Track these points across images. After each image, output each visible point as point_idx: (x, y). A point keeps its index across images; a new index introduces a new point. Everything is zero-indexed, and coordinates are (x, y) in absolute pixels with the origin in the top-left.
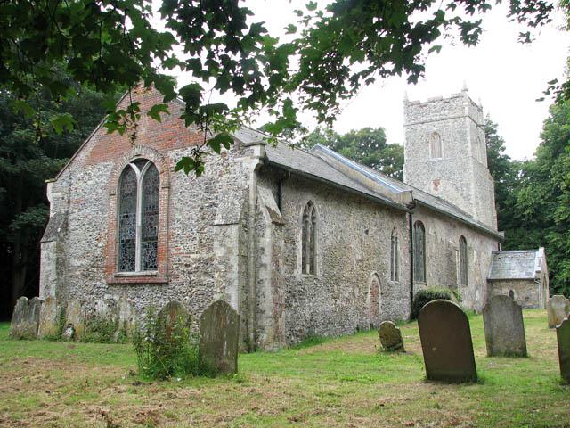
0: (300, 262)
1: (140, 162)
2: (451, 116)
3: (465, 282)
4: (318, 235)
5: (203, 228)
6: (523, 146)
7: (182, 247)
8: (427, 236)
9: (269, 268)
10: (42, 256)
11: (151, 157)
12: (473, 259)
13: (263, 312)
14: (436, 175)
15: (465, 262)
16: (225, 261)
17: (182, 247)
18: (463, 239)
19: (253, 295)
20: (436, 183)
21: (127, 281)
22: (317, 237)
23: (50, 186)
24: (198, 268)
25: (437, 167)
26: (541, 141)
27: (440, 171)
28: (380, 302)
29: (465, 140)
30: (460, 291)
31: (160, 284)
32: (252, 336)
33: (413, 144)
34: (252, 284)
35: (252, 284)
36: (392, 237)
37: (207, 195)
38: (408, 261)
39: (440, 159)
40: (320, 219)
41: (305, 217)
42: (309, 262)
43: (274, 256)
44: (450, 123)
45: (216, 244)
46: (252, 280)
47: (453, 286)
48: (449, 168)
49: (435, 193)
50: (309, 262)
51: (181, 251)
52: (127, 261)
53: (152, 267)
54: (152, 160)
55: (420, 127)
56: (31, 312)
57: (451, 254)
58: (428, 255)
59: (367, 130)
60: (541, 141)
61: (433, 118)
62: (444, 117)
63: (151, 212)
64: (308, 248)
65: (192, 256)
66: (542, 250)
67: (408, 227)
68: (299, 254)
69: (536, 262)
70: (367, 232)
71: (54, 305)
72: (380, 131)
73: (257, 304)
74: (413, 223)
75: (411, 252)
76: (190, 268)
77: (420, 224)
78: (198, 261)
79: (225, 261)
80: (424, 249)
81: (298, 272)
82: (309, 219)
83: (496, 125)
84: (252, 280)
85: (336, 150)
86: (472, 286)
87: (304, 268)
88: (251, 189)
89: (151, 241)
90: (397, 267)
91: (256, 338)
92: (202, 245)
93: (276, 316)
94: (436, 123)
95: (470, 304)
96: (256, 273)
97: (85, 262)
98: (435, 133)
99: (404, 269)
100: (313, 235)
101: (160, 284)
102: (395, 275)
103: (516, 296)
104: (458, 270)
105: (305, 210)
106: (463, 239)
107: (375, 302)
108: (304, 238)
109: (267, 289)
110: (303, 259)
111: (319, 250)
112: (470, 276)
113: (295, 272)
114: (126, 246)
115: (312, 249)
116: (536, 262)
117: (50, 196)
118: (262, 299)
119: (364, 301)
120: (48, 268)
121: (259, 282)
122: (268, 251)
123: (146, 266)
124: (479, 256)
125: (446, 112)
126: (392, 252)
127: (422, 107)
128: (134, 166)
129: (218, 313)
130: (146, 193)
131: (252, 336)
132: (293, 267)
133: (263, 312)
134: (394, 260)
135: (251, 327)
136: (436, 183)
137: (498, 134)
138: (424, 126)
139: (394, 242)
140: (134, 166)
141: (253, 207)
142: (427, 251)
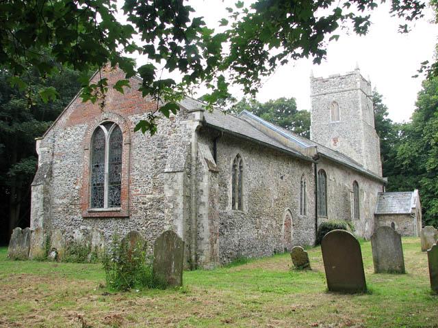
0: (230, 201)
1: (108, 124)
2: (346, 89)
3: (358, 216)
4: (245, 180)
5: (156, 175)
6: (402, 112)
7: (140, 189)
8: (328, 180)
9: (207, 206)
10: (32, 196)
11: (116, 120)
12: (363, 199)
13: (202, 239)
14: (335, 134)
15: (357, 201)
16: (173, 200)
17: (140, 189)
18: (356, 183)
19: (194, 226)
20: (335, 140)
21: (98, 216)
22: (244, 182)
23: (38, 143)
24: (152, 205)
25: (336, 128)
26: (416, 108)
27: (338, 131)
28: (292, 232)
29: (357, 107)
30: (353, 223)
31: (123, 218)
32: (193, 257)
33: (317, 110)
34: (193, 217)
35: (193, 217)
36: (302, 182)
37: (159, 150)
38: (313, 200)
39: (338, 122)
40: (246, 168)
41: (234, 166)
42: (237, 201)
43: (211, 196)
44: (346, 94)
45: (166, 187)
46: (194, 214)
47: (348, 219)
48: (345, 129)
49: (335, 148)
50: (237, 201)
51: (139, 192)
52: (97, 200)
53: (116, 204)
54: (117, 123)
55: (323, 97)
56: (24, 239)
57: (347, 195)
58: (329, 195)
59: (282, 99)
60: (416, 108)
61: (333, 91)
62: (341, 90)
63: (116, 162)
64: (236, 190)
65: (148, 196)
66: (416, 191)
67: (314, 174)
68: (230, 195)
69: (412, 200)
70: (282, 178)
71: (42, 234)
72: (292, 101)
73: (197, 233)
74: (317, 171)
75: (316, 193)
76: (146, 206)
77: (323, 172)
78: (153, 200)
79: (173, 200)
80: (326, 191)
81: (229, 208)
82: (237, 168)
83: (381, 96)
84: (194, 214)
85: (258, 115)
86: (362, 219)
87: (234, 205)
88: (193, 145)
89: (116, 185)
90: (305, 205)
91: (197, 259)
92: (155, 188)
93: (212, 243)
94: (335, 94)
95: (361, 233)
96: (197, 209)
97: (65, 201)
98: (335, 102)
99: (310, 206)
100: (240, 180)
101: (123, 218)
102: (303, 211)
103: (396, 227)
104: (352, 207)
105: (234, 161)
106: (356, 183)
107: (288, 232)
108: (234, 182)
109: (205, 221)
110: (233, 198)
111: (245, 191)
112: (361, 211)
113: (227, 208)
114: (97, 189)
115: (240, 191)
116: (412, 200)
117: (39, 151)
118: (201, 229)
119: (280, 230)
120: (37, 206)
121: (199, 216)
122: (206, 192)
123: (112, 204)
124: (368, 196)
125: (343, 86)
126: (301, 193)
127: (324, 82)
128: (103, 127)
129: (167, 240)
130: (112, 148)
131: (193, 257)
132: (225, 204)
133: (202, 239)
134: (303, 199)
135: (193, 251)
136: (335, 140)
137: (382, 102)
138: (326, 97)
139: (303, 185)
140: (103, 127)
141: (194, 159)
142: (328, 192)
